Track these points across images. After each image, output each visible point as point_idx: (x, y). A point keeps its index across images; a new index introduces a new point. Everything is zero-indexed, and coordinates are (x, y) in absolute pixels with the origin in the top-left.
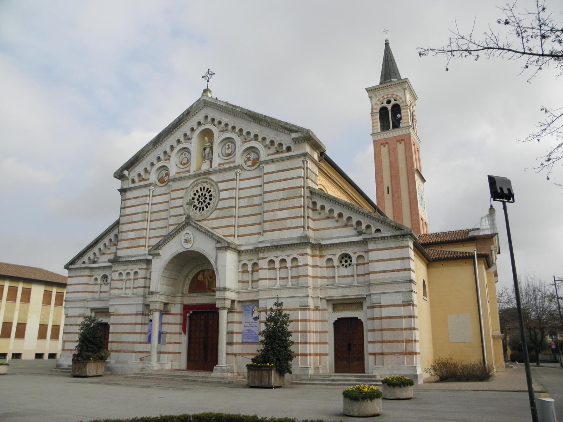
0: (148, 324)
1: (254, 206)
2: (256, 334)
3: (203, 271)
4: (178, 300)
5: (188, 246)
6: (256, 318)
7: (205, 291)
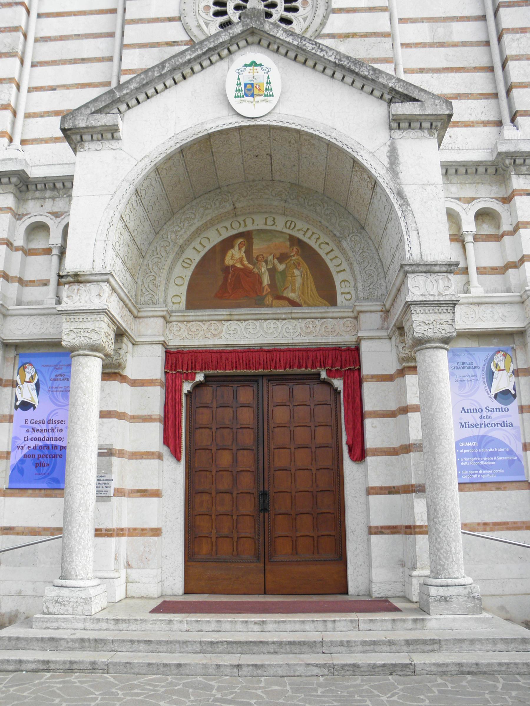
0: (10, 419)
1: (455, 45)
2: (511, 452)
3: (247, 236)
4: (150, 329)
5: (254, 110)
6: (506, 396)
7: (260, 303)
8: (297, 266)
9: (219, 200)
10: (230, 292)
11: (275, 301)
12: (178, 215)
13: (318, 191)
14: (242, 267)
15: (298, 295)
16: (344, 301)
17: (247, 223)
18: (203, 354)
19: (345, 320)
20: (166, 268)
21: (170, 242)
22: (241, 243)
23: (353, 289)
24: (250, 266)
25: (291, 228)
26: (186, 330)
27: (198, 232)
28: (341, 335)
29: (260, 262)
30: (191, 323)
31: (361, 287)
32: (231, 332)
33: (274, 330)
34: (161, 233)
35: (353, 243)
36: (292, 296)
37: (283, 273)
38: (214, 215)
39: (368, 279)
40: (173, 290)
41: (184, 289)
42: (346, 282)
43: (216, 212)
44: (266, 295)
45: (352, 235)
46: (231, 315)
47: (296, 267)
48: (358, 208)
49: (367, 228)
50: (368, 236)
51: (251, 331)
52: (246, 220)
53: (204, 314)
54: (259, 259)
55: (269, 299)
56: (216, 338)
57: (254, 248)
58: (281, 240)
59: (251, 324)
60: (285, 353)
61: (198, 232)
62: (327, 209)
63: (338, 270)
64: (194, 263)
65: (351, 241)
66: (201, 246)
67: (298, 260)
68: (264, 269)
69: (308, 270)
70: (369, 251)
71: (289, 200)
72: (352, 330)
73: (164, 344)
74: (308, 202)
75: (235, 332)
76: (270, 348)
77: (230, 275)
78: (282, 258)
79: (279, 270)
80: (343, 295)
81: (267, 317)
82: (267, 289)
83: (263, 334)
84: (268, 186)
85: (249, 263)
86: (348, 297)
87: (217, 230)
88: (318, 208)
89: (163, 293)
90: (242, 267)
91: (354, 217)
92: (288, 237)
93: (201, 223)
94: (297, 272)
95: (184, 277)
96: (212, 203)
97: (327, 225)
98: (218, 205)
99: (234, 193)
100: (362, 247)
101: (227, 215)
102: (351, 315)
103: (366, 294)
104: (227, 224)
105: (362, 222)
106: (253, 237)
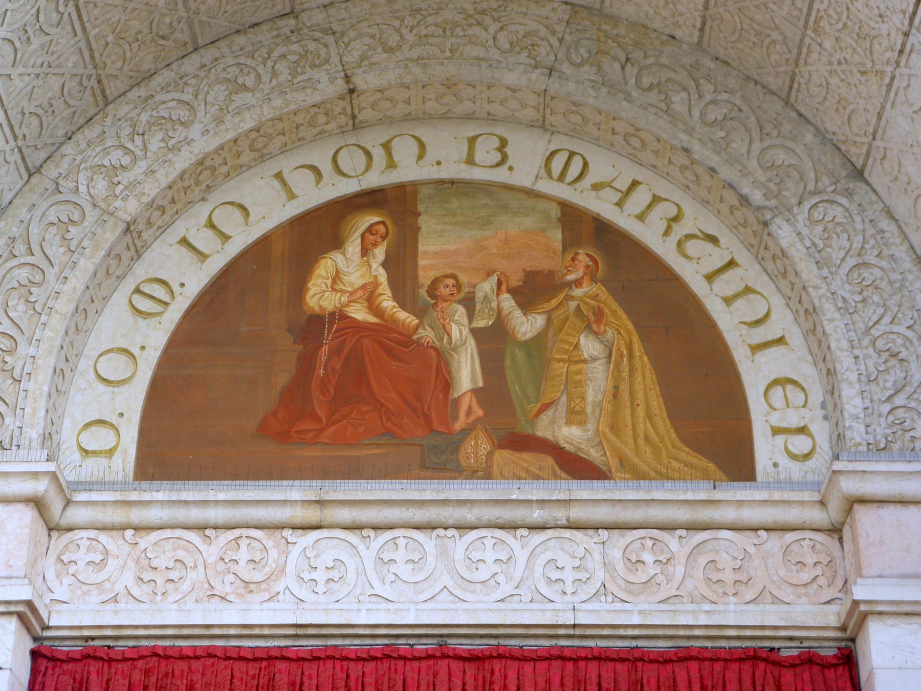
3: (396, 206)
7: (440, 459)
8: (592, 321)
9: (294, 58)
10: (321, 413)
11: (502, 456)
12: (126, 108)
13: (678, 33)
14: (373, 320)
15: (597, 432)
16: (783, 461)
17: (396, 157)
18: (195, 665)
19: (790, 537)
20: (64, 306)
21: (88, 208)
22: (370, 230)
23: (820, 413)
24: (402, 315)
25: (570, 177)
26: (131, 564)
27: (204, 177)
28: (776, 600)
29: (442, 305)
30: (155, 536)
31: (858, 401)
32: (321, 576)
33: (496, 568)
34: (51, 171)
35: (819, 229)
36: (570, 435)
37: (537, 346)
38: (268, 113)
39: (886, 371)
40: (85, 400)
41: (133, 399)
42: (789, 388)
43: (278, 102)
44: (467, 431)
45: (816, 199)
46: (320, 503)
47: (589, 327)
48: (843, 91)
49: (875, 175)
50: (880, 206)
51: (404, 571)
52: (394, 144)
53: (211, 496)
54: (443, 291)
55: (478, 447)
56: (257, 598)
57: (421, 248)
58: (529, 222)
59: (402, 542)
60: (542, 666)
61: (204, 177)
62: (714, 102)
63: (756, 341)
64: (179, 299)
65: (812, 222)
66: (210, 233)
67: (595, 297)
68: (459, 329)
69: (636, 339)
70: (883, 264)
71: (566, 68)
72: (822, 581)
73: (27, 615)
74: (638, 77)
75: (335, 575)
76: (478, 645)
77: (325, 349)
78: (533, 290)
79: (521, 337)
80: (780, 439)
81: (469, 515)
82: (469, 409)
83: (450, 584)
84: (483, 12)
85: (403, 306)
86: (800, 444)
87: (279, 176)
88: (676, 99)
89: (42, 404)
90: (373, 320)
91: (819, 132)
92: (555, 212)
93: (213, 143)
94: (590, 346)
95: (136, 351)
96: (260, 69)
97: (714, 160)
98: (284, 76)
99: (352, 34)
100: (857, 245)
101: (322, 119)
102: (816, 516)
103: (881, 430)
104: (321, 157)
105: (854, 151)
106: (421, 208)
